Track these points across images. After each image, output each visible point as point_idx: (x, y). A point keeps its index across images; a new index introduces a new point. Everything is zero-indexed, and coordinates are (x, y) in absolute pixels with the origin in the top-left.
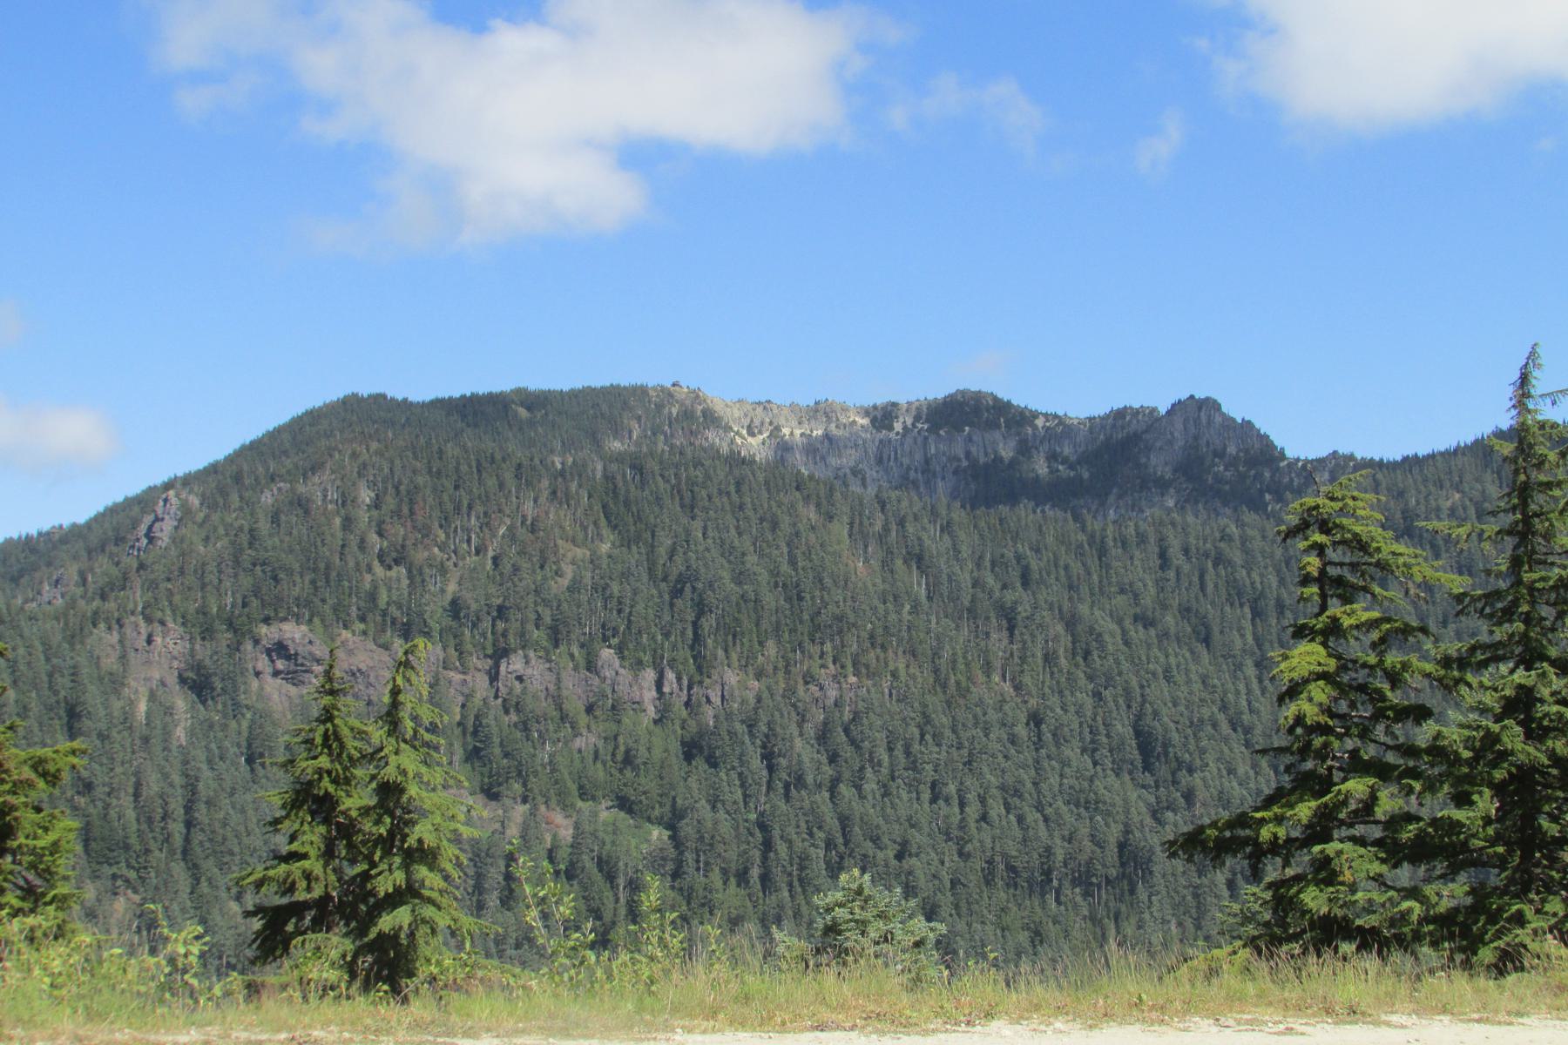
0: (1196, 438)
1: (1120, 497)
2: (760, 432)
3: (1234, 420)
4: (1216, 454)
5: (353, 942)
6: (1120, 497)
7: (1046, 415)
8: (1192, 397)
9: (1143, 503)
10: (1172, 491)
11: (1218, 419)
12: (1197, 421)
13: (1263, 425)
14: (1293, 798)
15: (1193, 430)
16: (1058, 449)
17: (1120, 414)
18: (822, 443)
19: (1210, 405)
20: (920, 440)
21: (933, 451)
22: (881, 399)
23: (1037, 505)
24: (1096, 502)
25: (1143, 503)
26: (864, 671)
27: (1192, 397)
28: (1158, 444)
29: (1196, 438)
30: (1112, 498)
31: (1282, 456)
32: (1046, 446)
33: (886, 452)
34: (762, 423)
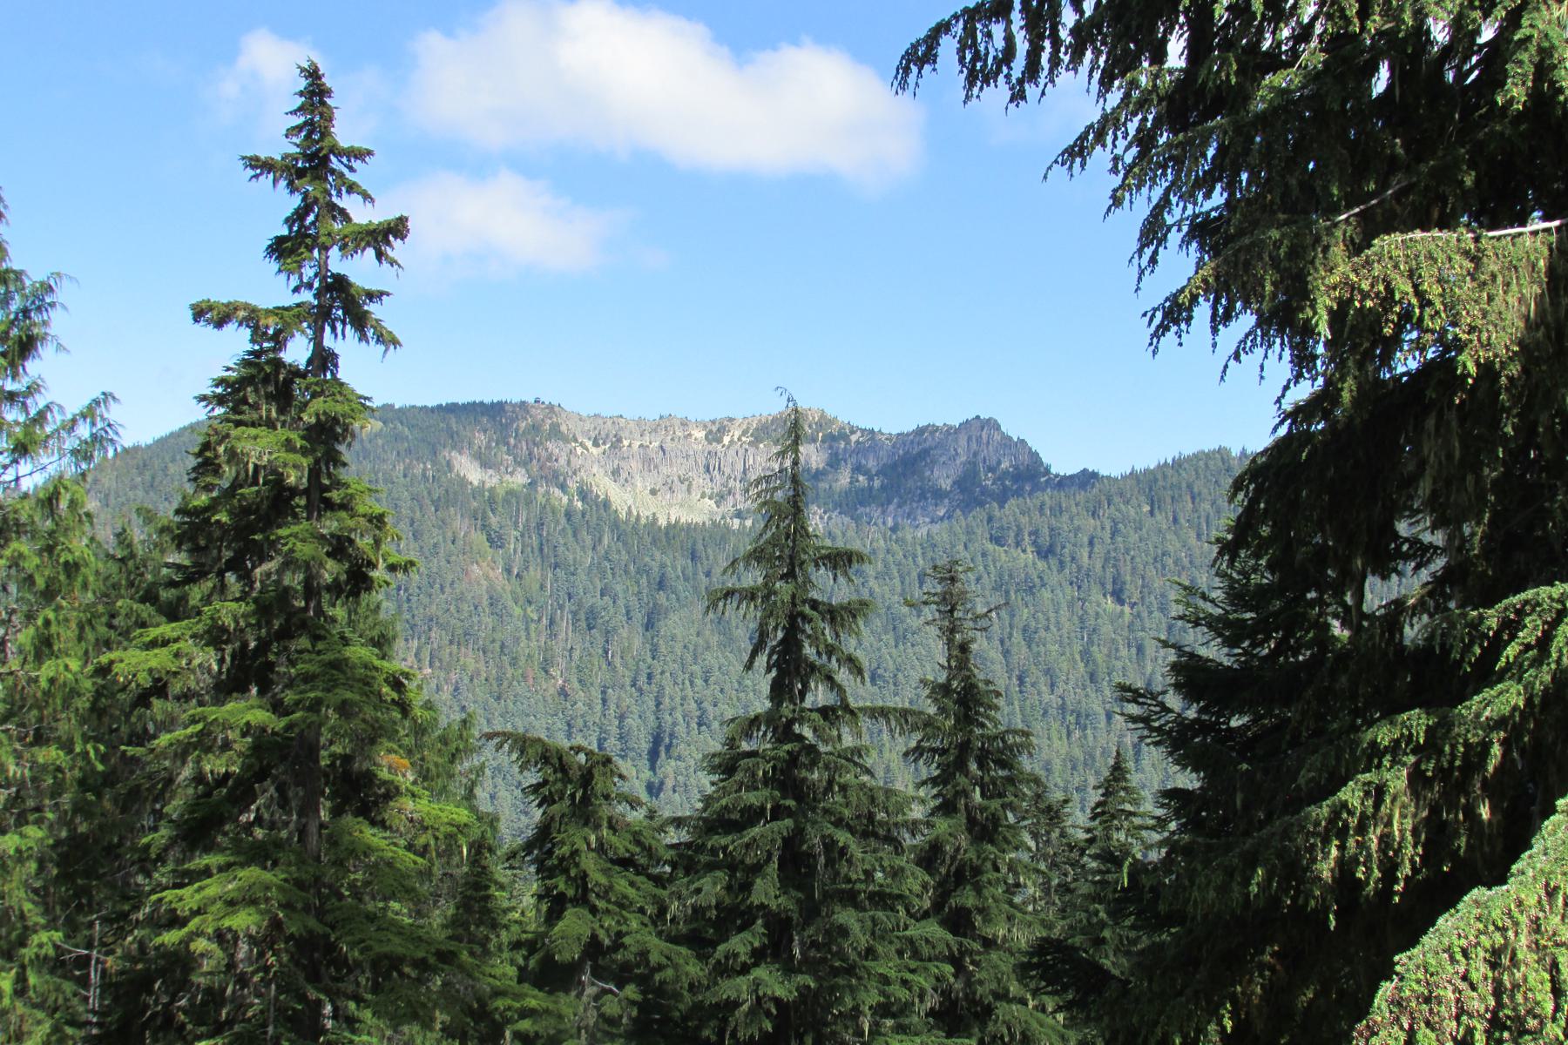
0: (975, 454)
1: (899, 506)
2: (604, 443)
3: (1010, 439)
4: (991, 469)
5: (752, 903)
6: (899, 506)
7: (863, 431)
8: (978, 417)
9: (919, 511)
10: (946, 501)
11: (997, 437)
12: (979, 439)
13: (1034, 445)
14: (249, 774)
15: (974, 446)
16: (864, 462)
17: (920, 431)
18: (657, 453)
19: (992, 425)
20: (741, 452)
21: (751, 462)
22: (720, 415)
23: (825, 512)
24: (879, 510)
25: (919, 511)
26: (438, 664)
27: (978, 417)
28: (942, 459)
29: (975, 454)
30: (891, 507)
31: (1047, 471)
32: (854, 460)
33: (712, 462)
34: (607, 436)
